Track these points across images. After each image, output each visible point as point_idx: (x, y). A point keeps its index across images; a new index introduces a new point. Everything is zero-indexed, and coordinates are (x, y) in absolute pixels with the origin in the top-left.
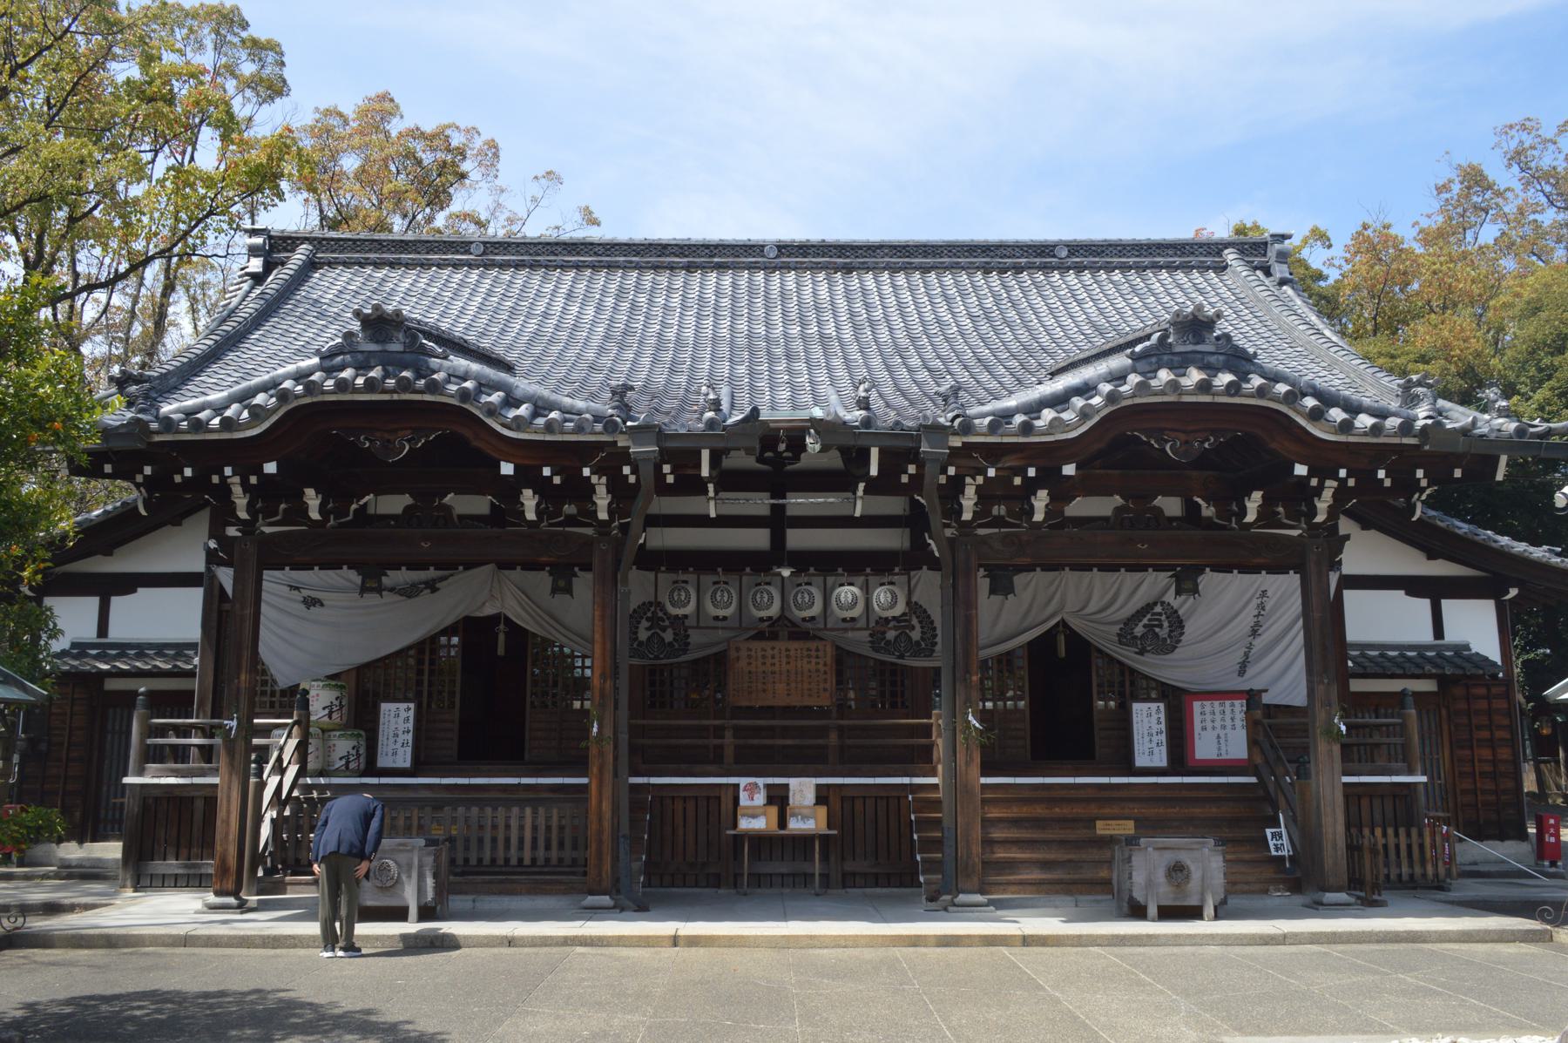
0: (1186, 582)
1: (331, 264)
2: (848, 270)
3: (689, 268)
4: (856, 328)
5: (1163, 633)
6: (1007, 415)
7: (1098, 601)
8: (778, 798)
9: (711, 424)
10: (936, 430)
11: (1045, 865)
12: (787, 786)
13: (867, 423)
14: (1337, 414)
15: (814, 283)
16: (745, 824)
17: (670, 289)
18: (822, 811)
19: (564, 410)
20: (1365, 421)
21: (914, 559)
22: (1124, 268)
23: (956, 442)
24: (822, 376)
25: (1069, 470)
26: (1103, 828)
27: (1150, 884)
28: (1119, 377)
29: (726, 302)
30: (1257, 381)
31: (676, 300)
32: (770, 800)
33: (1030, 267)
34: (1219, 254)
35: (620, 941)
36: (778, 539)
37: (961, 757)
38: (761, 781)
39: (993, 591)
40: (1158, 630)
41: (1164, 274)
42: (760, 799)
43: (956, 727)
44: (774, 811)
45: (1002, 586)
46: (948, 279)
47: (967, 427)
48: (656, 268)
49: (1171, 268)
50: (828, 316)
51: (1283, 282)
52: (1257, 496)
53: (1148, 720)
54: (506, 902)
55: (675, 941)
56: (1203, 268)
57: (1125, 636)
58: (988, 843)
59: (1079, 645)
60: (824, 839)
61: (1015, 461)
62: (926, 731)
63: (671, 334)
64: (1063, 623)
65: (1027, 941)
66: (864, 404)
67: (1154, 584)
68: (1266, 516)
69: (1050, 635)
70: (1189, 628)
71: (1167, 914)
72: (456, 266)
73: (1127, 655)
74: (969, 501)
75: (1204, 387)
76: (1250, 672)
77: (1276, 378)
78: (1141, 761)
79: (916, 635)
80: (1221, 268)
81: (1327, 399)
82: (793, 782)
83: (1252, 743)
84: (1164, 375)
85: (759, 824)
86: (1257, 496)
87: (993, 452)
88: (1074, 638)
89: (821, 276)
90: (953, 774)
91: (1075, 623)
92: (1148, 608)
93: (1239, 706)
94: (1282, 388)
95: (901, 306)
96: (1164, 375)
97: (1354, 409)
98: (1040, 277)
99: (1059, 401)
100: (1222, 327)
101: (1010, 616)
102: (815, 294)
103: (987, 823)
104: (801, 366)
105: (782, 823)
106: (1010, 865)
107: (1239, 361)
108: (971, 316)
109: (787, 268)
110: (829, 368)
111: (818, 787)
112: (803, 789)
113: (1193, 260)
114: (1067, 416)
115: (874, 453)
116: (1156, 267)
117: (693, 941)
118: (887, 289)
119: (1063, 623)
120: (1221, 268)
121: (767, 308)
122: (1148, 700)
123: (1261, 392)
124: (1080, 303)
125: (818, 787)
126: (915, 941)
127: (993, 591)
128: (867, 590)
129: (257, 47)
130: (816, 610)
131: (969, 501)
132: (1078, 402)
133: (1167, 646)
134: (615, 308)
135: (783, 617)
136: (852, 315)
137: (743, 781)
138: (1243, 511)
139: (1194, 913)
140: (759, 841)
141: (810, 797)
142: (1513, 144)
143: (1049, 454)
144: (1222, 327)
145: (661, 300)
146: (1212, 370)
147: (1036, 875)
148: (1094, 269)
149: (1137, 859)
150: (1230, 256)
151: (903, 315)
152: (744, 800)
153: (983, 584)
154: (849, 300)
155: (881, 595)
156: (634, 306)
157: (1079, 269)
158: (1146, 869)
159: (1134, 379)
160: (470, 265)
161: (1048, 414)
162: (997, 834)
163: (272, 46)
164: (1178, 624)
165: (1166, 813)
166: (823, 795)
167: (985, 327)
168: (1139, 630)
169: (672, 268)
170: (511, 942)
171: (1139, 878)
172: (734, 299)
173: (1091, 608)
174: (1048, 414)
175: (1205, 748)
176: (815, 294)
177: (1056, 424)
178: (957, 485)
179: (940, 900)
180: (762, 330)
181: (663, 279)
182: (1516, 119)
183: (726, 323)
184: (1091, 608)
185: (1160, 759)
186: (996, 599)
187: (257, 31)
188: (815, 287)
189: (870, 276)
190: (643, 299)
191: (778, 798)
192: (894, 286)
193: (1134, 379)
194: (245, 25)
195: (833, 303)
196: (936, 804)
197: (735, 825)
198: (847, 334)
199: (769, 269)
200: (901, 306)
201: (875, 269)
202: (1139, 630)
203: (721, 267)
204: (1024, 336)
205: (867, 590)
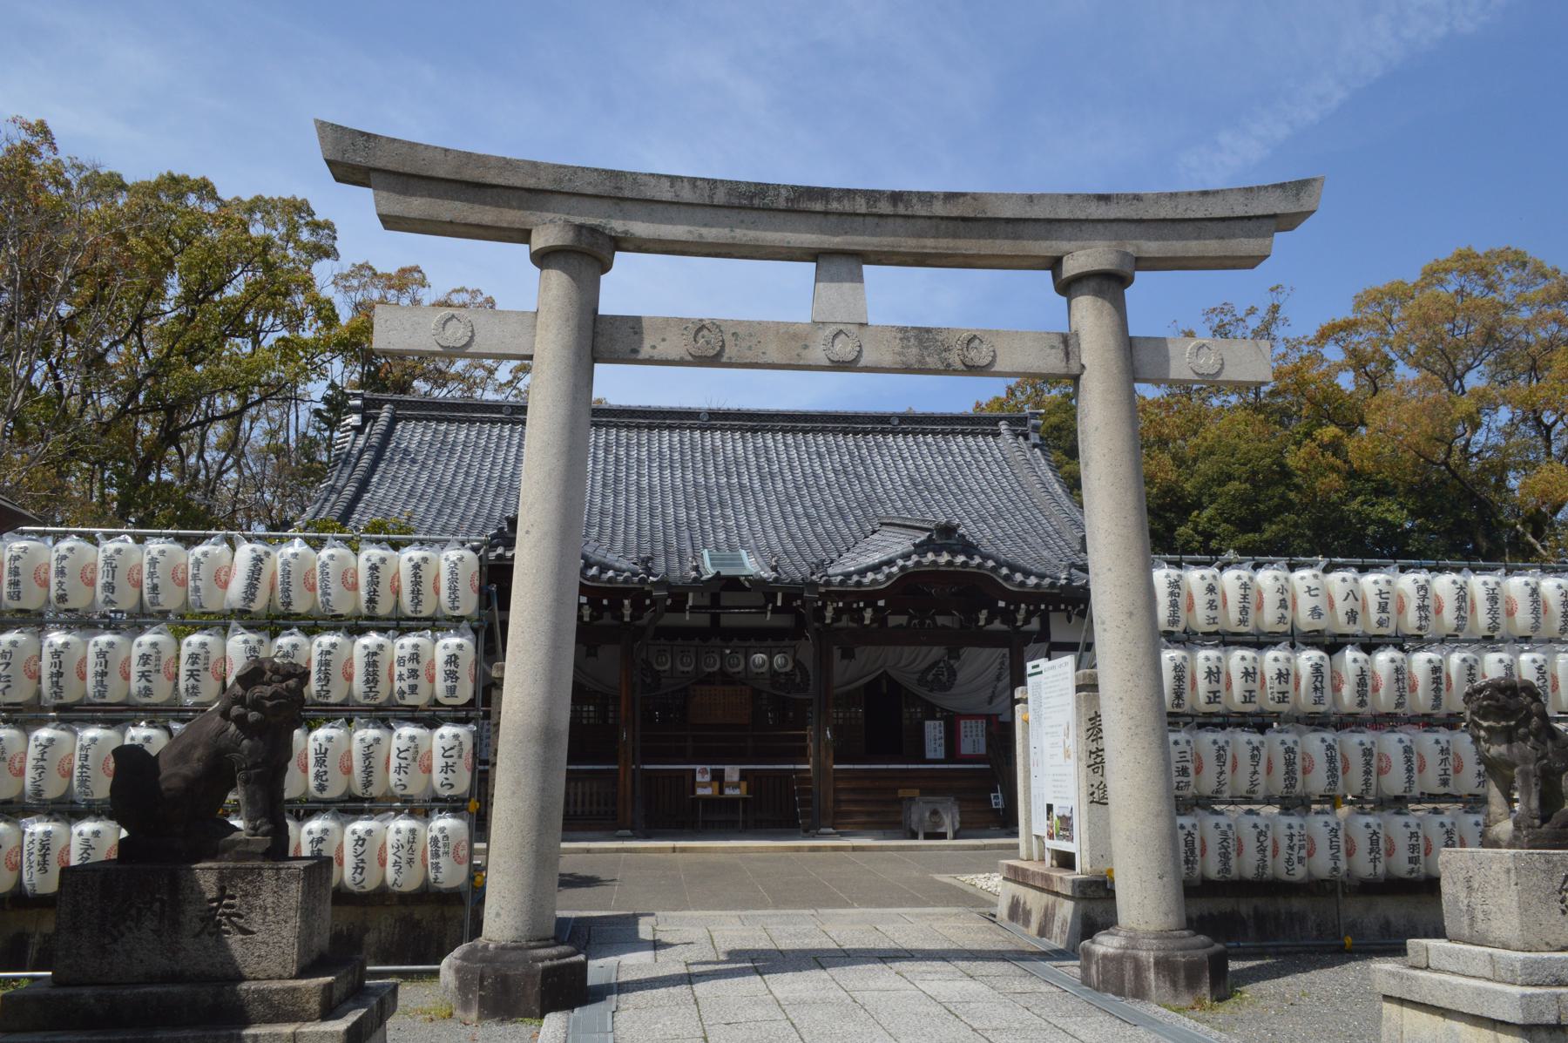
0: (954, 653)
1: (408, 419)
2: (754, 431)
3: (650, 428)
4: (762, 479)
5: (944, 679)
6: (848, 575)
7: (908, 662)
8: (718, 777)
9: (695, 579)
10: (814, 584)
11: (869, 814)
12: (723, 771)
13: (776, 580)
14: (1019, 577)
15: (734, 440)
16: (700, 792)
17: (639, 444)
18: (744, 785)
19: (616, 570)
20: (1032, 581)
21: (796, 633)
22: (934, 433)
23: (822, 590)
24: (742, 518)
25: (881, 603)
26: (901, 793)
27: (921, 820)
28: (906, 556)
29: (677, 456)
30: (977, 560)
31: (644, 454)
32: (713, 778)
33: (873, 432)
34: (996, 424)
35: (646, 850)
36: (715, 619)
37: (823, 754)
38: (708, 767)
39: (843, 657)
40: (943, 678)
41: (960, 438)
42: (707, 778)
43: (820, 736)
44: (716, 785)
45: (848, 654)
46: (820, 438)
47: (828, 583)
48: (628, 427)
49: (964, 433)
50: (743, 469)
51: (1035, 446)
52: (985, 612)
53: (934, 731)
54: (590, 834)
55: (674, 850)
56: (985, 434)
57: (922, 681)
58: (837, 802)
59: (895, 685)
60: (745, 800)
61: (852, 596)
62: (804, 738)
63: (645, 482)
64: (885, 672)
65: (854, 849)
66: (774, 569)
67: (937, 652)
68: (989, 621)
69: (877, 680)
70: (961, 677)
71: (928, 836)
72: (493, 422)
73: (923, 692)
74: (829, 613)
75: (950, 563)
76: (995, 702)
77: (985, 557)
78: (929, 755)
79: (798, 679)
80: (996, 434)
81: (1014, 568)
82: (727, 768)
83: (989, 745)
84: (930, 556)
85: (708, 792)
86: (985, 612)
87: (841, 595)
88: (893, 683)
89: (737, 435)
90: (818, 763)
91: (893, 673)
92: (936, 664)
93: (982, 724)
94: (991, 563)
95: (790, 460)
96: (930, 556)
97: (1027, 574)
98: (880, 438)
99: (876, 568)
100: (962, 530)
101: (849, 672)
102: (734, 449)
103: (836, 791)
104: (729, 512)
105: (721, 791)
106: (849, 814)
107: (969, 549)
108: (834, 470)
109: (713, 429)
110: (747, 514)
111: (742, 771)
112: (732, 772)
113: (979, 428)
114: (880, 577)
115: (780, 596)
116: (954, 433)
117: (683, 850)
118: (781, 447)
119: (885, 672)
120: (996, 434)
121: (704, 461)
122: (934, 718)
123: (979, 566)
124: (904, 460)
125: (742, 771)
126: (798, 849)
127: (843, 657)
128: (771, 658)
129: (316, 226)
130: (741, 667)
131: (829, 613)
132: (886, 569)
133: (946, 687)
134: (606, 461)
135: (722, 671)
136: (759, 468)
137: (698, 767)
138: (978, 620)
139: (943, 836)
140: (707, 800)
141: (736, 778)
142: (1217, 321)
143: (870, 597)
144: (962, 530)
145: (634, 453)
146: (954, 553)
147: (863, 819)
148: (915, 433)
149: (913, 809)
150: (1003, 426)
151: (791, 469)
152: (699, 778)
153: (837, 653)
154: (757, 456)
155: (778, 660)
156: (617, 459)
157: (905, 433)
158: (919, 813)
159: (915, 558)
160: (503, 422)
161: (870, 576)
162: (843, 797)
163: (329, 226)
164: (953, 674)
165: (935, 785)
166: (744, 775)
167: (843, 480)
168: (930, 677)
169: (638, 427)
170: (588, 851)
171: (915, 818)
172: (682, 453)
173: (903, 663)
174: (870, 576)
175: (966, 748)
176: (734, 449)
177: (874, 581)
178: (824, 606)
179: (810, 831)
180: (702, 480)
181: (633, 434)
182: (1218, 304)
183: (678, 473)
184: (903, 663)
185: (941, 754)
186: (845, 662)
187: (319, 217)
188: (731, 444)
189: (769, 436)
190: (622, 452)
191: (718, 777)
192: (785, 444)
193: (915, 558)
194: (312, 214)
195: (746, 458)
196: (809, 780)
197: (694, 792)
198: (757, 485)
199: (703, 429)
200: (790, 460)
201: (774, 431)
202: (930, 677)
203: (671, 428)
204: (868, 489)
205: (771, 658)
